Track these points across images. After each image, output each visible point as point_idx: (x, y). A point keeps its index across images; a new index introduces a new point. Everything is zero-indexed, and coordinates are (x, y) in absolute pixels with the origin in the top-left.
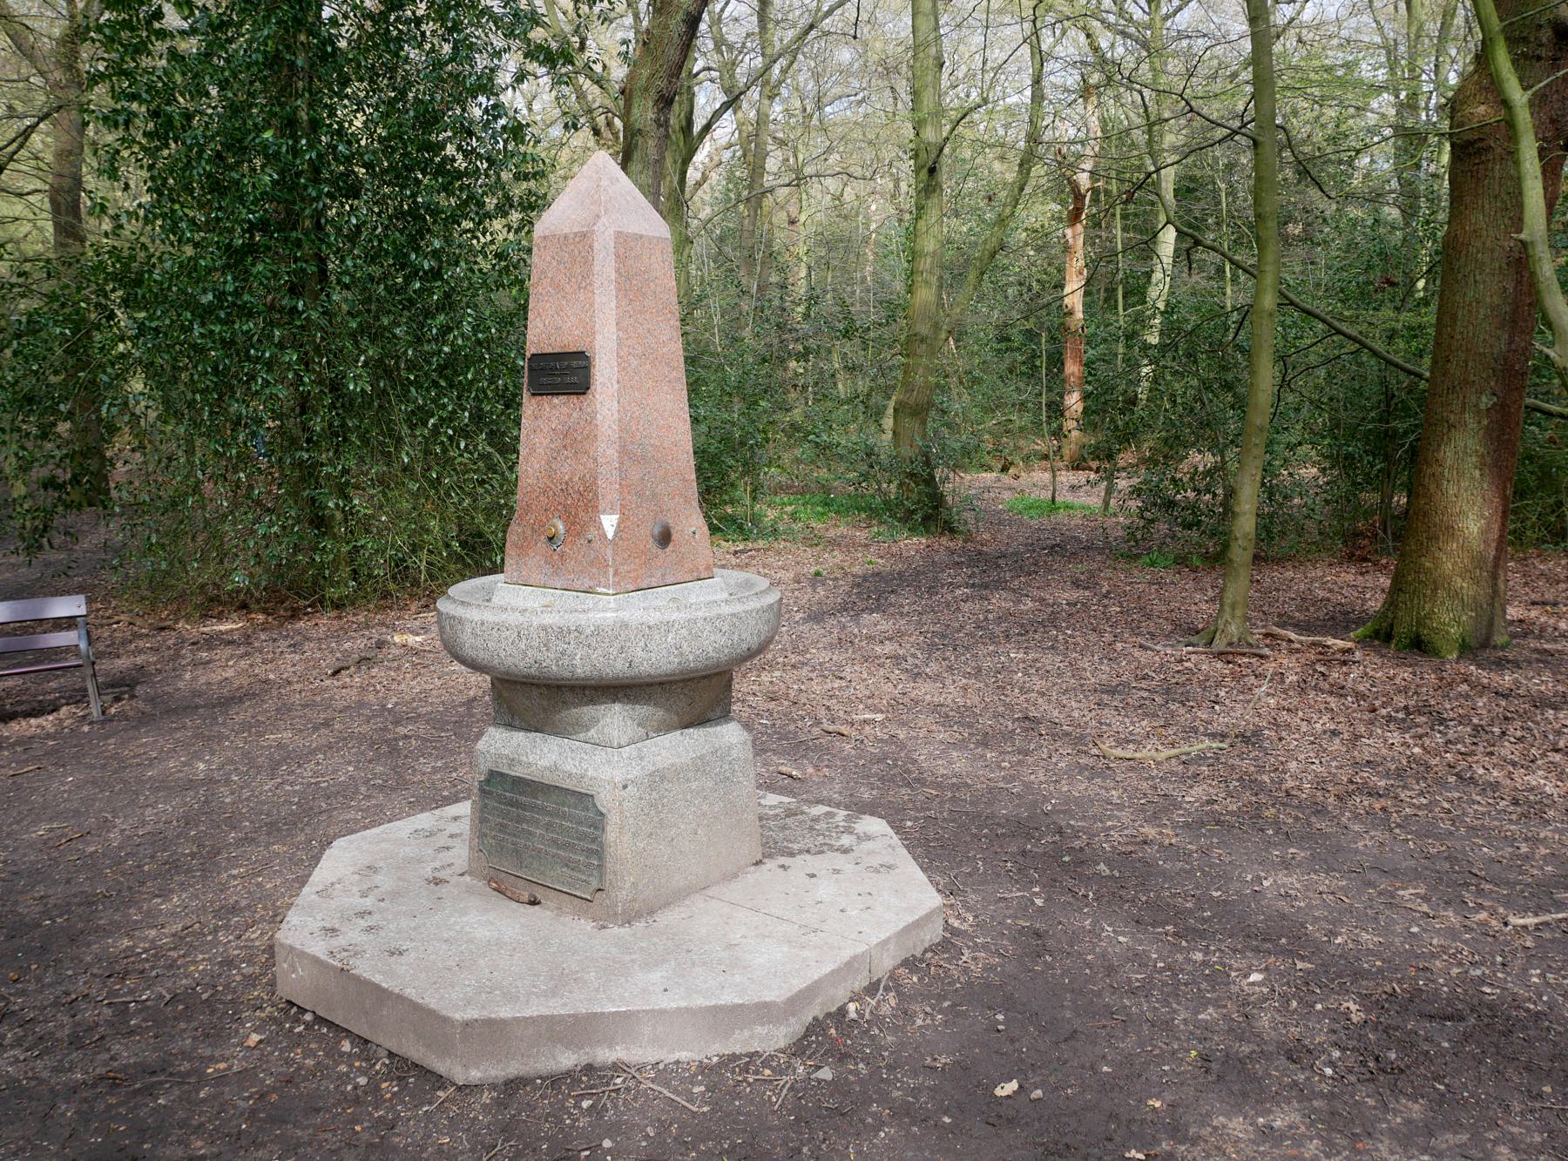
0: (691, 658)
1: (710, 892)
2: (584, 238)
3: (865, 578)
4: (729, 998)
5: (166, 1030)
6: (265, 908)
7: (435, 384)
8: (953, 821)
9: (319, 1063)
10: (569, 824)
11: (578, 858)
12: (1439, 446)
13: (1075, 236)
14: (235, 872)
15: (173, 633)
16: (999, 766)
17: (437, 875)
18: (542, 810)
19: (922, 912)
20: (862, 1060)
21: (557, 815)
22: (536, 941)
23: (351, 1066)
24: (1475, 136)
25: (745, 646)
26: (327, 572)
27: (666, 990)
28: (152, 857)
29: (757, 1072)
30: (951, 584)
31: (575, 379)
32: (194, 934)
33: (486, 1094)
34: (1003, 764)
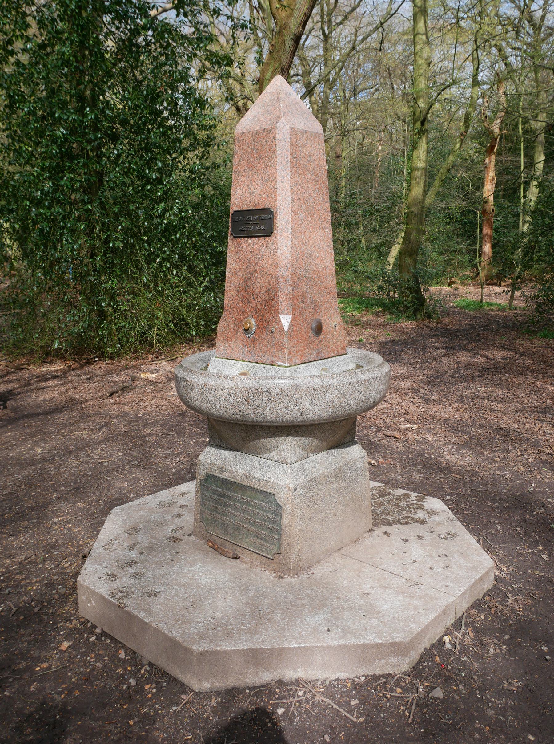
0: (340, 409)
1: (344, 551)
2: (270, 131)
3: (386, 343)
4: (371, 638)
5: (13, 635)
6: (73, 546)
7: (160, 240)
8: (474, 497)
9: (105, 666)
10: (258, 511)
11: (264, 532)
13: (491, 161)
14: (56, 520)
15: (27, 371)
16: (493, 460)
17: (174, 534)
18: (241, 501)
19: (483, 571)
20: (461, 682)
21: (251, 504)
22: (240, 588)
23: (125, 669)
25: (372, 400)
26: (105, 340)
27: (329, 630)
28: (10, 509)
29: (392, 690)
30: (434, 346)
31: (263, 227)
32: (31, 563)
33: (213, 700)
34: (496, 459)
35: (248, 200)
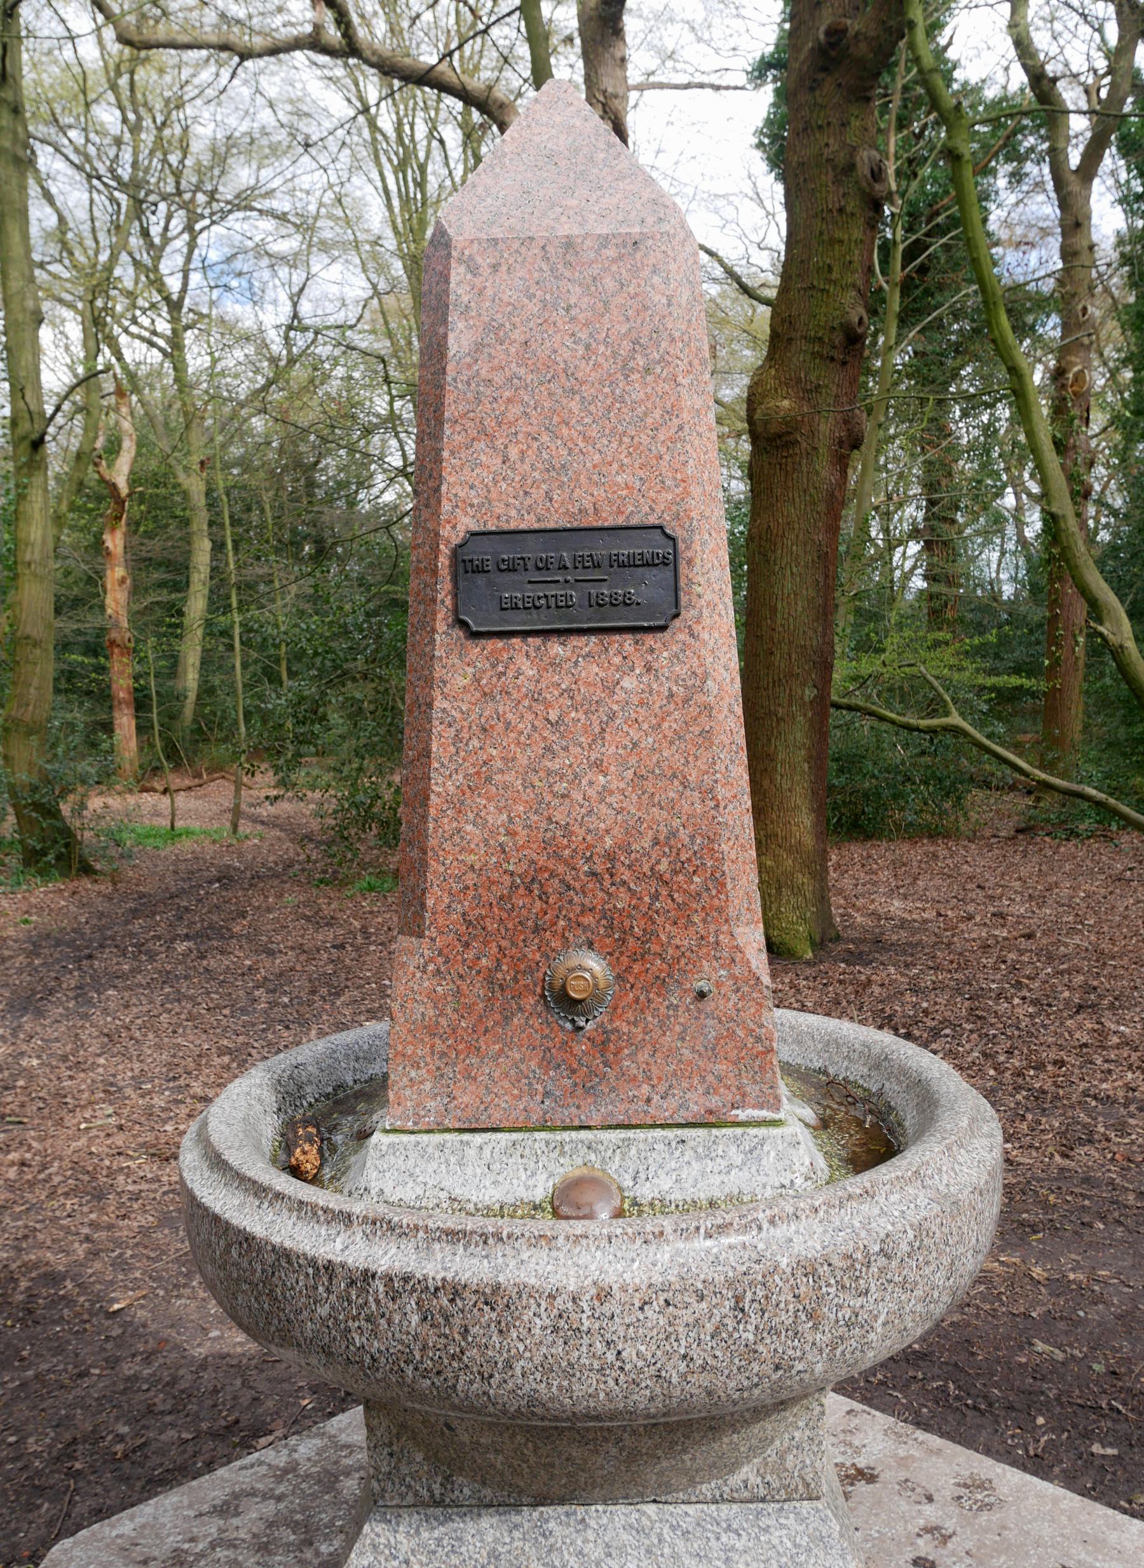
12: (769, 740)
24: (784, 428)
35: (538, 494)
